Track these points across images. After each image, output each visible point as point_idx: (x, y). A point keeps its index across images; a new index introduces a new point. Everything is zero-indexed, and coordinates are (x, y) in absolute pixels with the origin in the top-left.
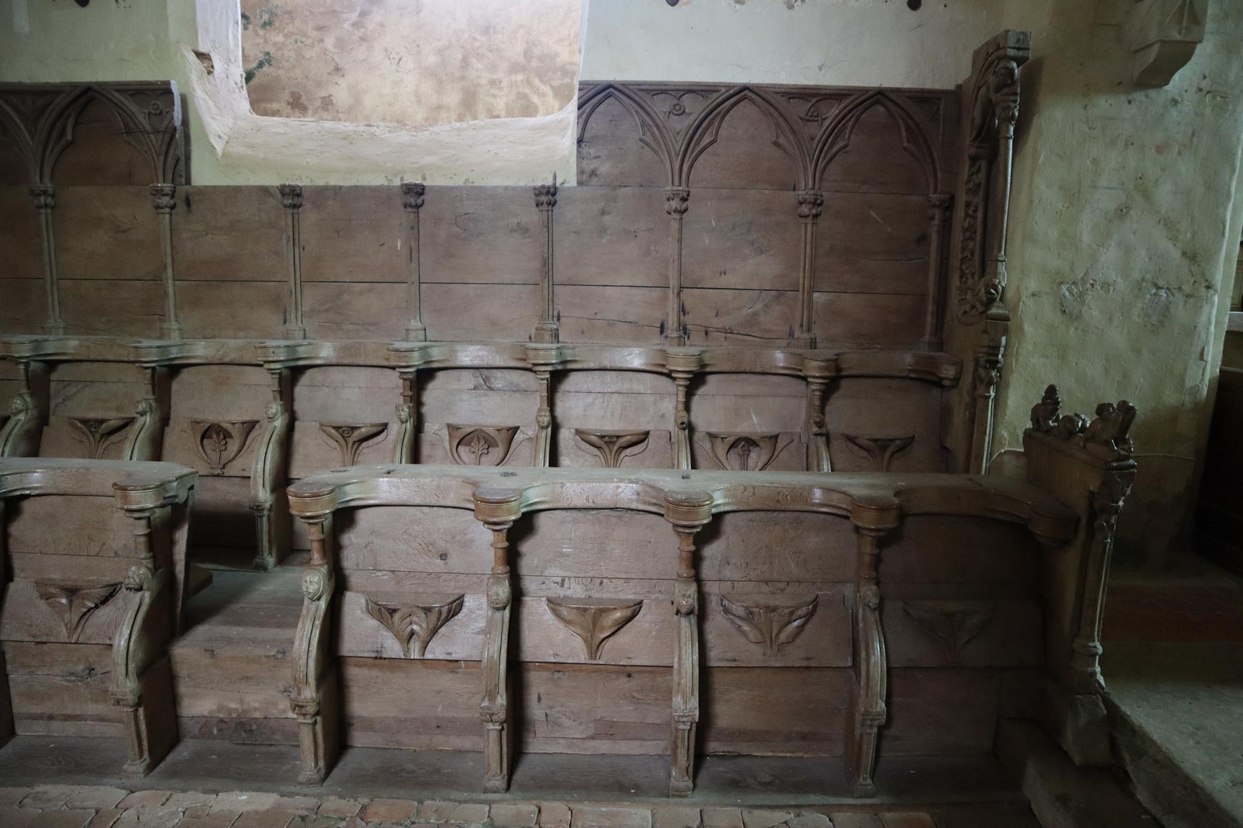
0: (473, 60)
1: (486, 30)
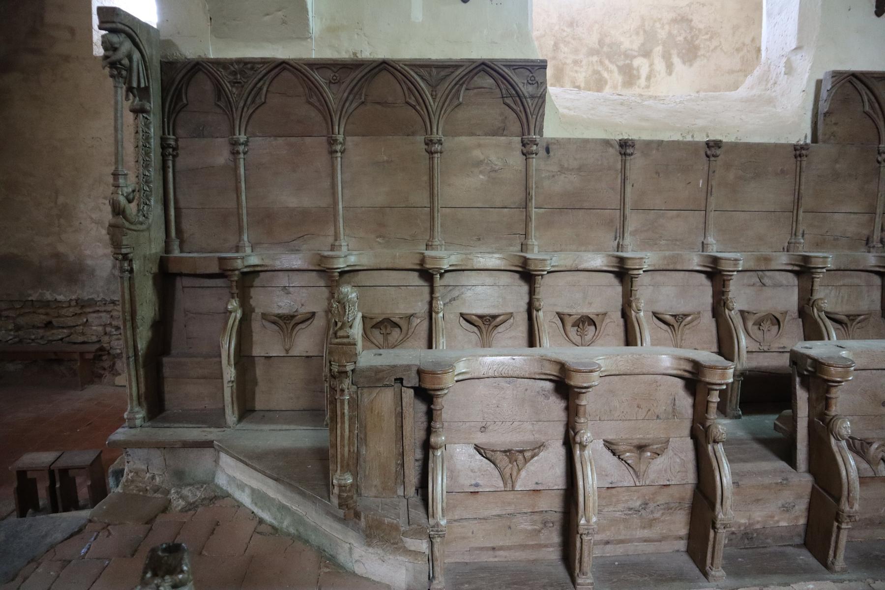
0: (562, 45)
1: (572, 24)
